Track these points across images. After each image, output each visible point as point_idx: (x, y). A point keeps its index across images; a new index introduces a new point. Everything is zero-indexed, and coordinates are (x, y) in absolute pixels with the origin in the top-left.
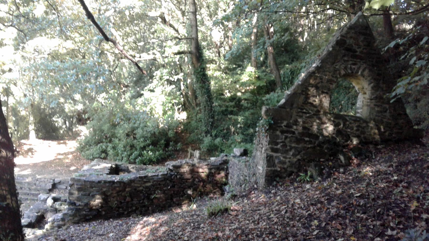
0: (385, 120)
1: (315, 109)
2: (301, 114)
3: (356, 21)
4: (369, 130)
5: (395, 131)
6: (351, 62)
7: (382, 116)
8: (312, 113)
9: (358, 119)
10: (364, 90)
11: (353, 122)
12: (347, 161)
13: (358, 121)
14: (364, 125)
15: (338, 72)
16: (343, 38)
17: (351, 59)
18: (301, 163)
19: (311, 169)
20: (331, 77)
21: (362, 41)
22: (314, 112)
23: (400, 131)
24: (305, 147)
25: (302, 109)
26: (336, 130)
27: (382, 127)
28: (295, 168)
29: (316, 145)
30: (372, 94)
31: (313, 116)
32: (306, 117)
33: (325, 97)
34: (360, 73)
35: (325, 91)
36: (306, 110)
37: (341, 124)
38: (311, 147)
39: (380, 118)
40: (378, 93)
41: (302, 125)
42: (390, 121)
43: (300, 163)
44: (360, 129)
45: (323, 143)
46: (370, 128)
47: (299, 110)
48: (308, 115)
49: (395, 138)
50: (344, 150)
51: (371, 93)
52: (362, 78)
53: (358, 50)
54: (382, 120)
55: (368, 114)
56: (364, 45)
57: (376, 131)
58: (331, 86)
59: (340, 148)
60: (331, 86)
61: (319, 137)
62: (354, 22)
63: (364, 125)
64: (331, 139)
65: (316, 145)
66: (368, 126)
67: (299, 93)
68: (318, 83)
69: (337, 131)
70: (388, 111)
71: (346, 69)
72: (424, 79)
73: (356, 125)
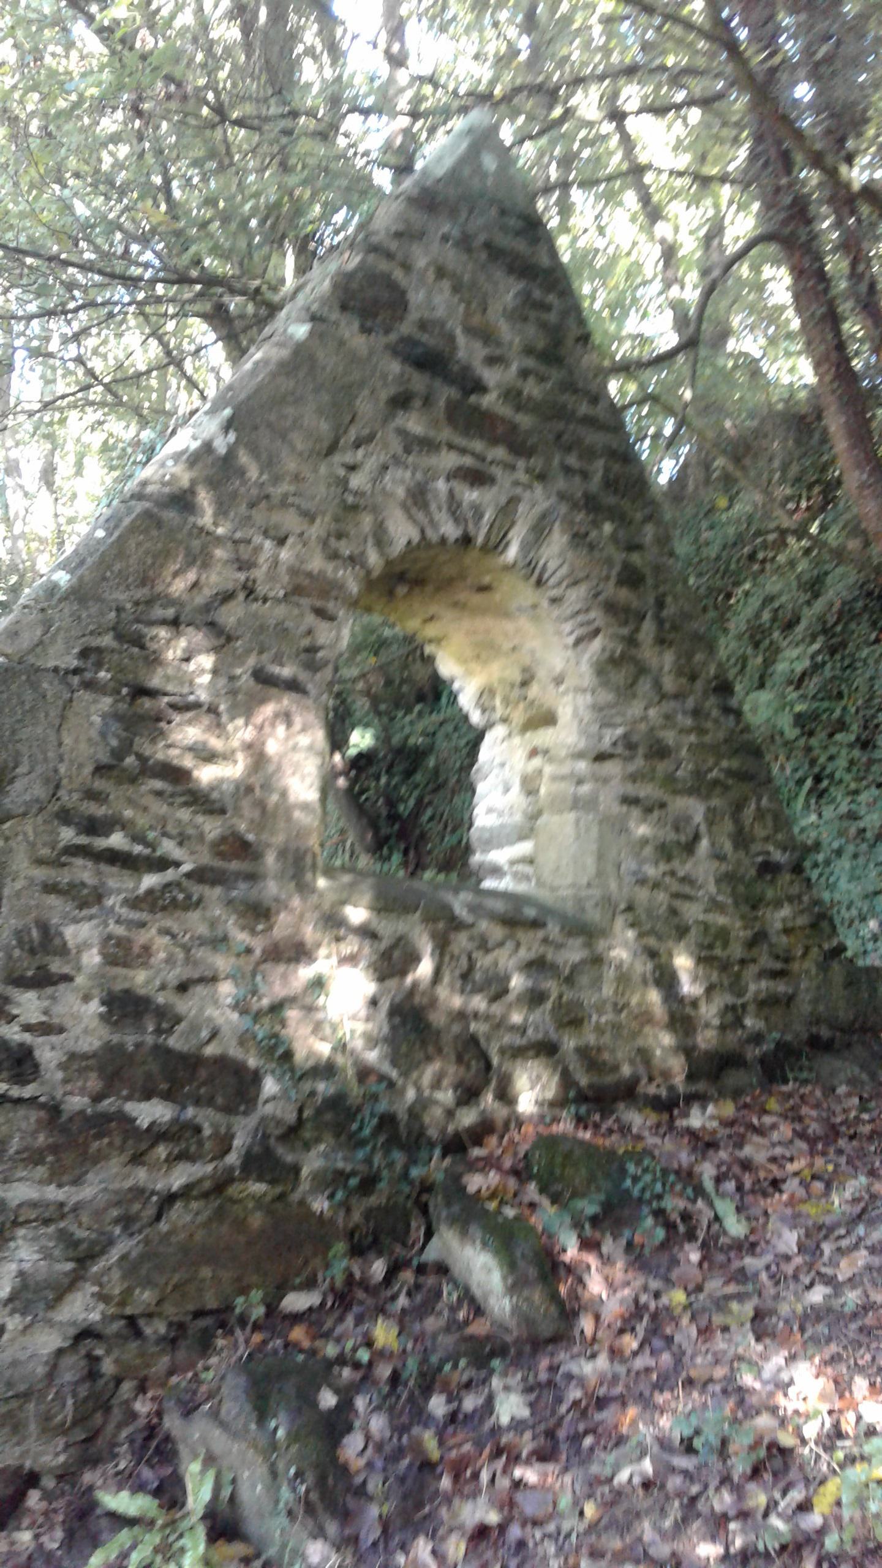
0: (692, 912)
1: (212, 828)
2: (83, 872)
3: (462, 161)
4: (608, 990)
5: (752, 987)
6: (449, 460)
7: (676, 887)
8: (186, 868)
9: (530, 912)
10: (534, 691)
11: (497, 932)
12: (537, 1295)
13: (536, 924)
14: (573, 954)
15: (367, 521)
16: (384, 266)
17: (446, 434)
18: (108, 1367)
19: (219, 1440)
20: (317, 563)
21: (518, 316)
22: (206, 858)
23: (781, 987)
24: (139, 1193)
25: (94, 827)
26: (385, 1005)
27: (683, 962)
28: (49, 1428)
29: (233, 1158)
30: (603, 715)
31: (197, 890)
32: (134, 903)
33: (287, 718)
34: (512, 552)
35: (286, 671)
36: (138, 838)
37: (414, 959)
38: (185, 1193)
39: (662, 897)
40: (636, 709)
41: (98, 976)
42: (721, 920)
43: (93, 1360)
44: (551, 986)
45: (292, 1133)
46: (610, 974)
47: (68, 835)
48: (150, 881)
49: (757, 1038)
50: (475, 1182)
51: (597, 708)
52: (525, 594)
53: (491, 376)
54: (673, 912)
55: (590, 862)
56: (529, 351)
57: (654, 996)
58: (324, 634)
59: (436, 1167)
60: (324, 634)
61: (256, 1078)
62: (448, 163)
63: (573, 954)
64: (355, 1091)
65: (233, 1158)
66: (597, 961)
67: (62, 675)
68: (227, 597)
69: (394, 1011)
70: (704, 844)
71: (424, 506)
72: (264, 952)
73: (524, 954)
